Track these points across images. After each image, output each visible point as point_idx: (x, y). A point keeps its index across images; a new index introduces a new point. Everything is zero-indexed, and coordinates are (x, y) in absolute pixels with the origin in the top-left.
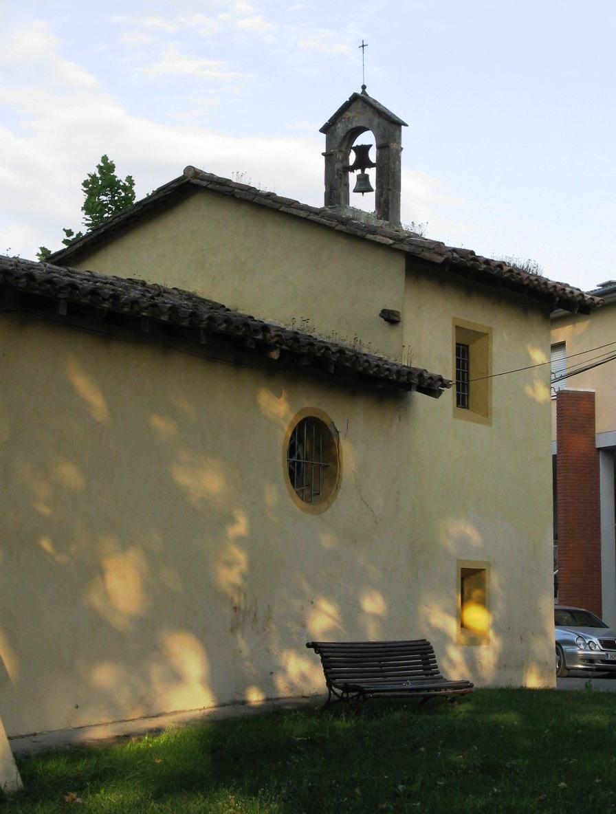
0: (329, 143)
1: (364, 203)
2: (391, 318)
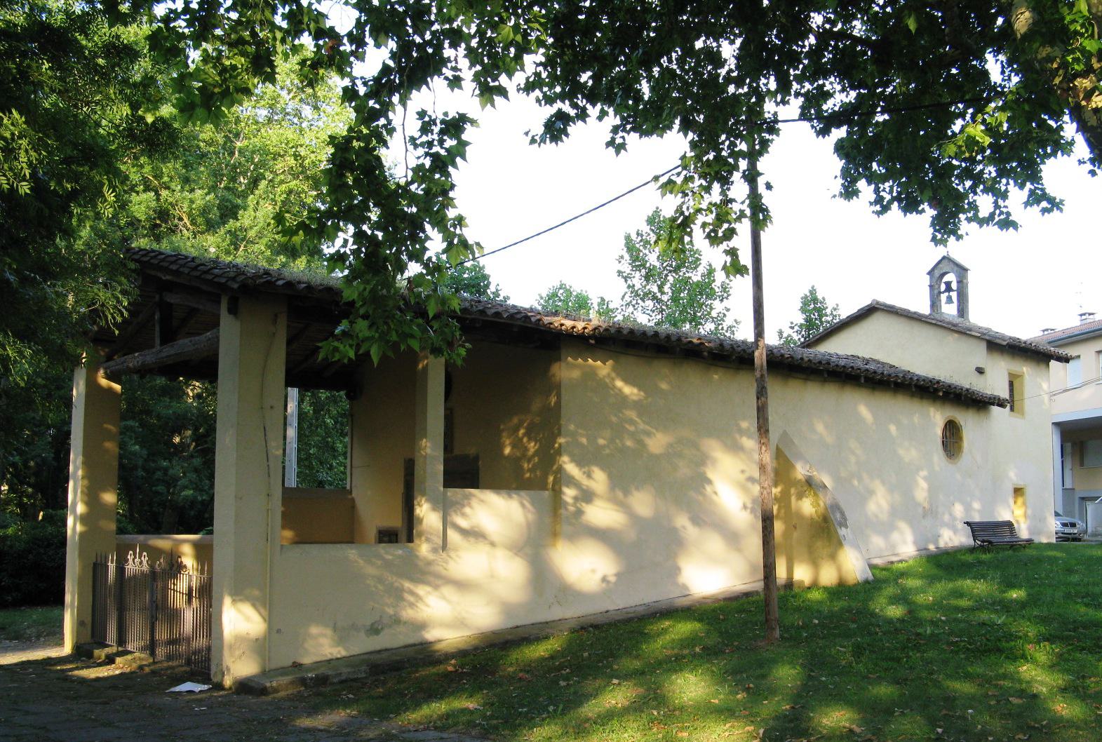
0: (931, 279)
1: (949, 310)
2: (980, 371)
